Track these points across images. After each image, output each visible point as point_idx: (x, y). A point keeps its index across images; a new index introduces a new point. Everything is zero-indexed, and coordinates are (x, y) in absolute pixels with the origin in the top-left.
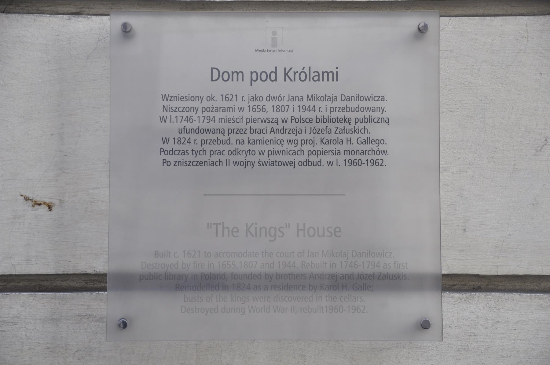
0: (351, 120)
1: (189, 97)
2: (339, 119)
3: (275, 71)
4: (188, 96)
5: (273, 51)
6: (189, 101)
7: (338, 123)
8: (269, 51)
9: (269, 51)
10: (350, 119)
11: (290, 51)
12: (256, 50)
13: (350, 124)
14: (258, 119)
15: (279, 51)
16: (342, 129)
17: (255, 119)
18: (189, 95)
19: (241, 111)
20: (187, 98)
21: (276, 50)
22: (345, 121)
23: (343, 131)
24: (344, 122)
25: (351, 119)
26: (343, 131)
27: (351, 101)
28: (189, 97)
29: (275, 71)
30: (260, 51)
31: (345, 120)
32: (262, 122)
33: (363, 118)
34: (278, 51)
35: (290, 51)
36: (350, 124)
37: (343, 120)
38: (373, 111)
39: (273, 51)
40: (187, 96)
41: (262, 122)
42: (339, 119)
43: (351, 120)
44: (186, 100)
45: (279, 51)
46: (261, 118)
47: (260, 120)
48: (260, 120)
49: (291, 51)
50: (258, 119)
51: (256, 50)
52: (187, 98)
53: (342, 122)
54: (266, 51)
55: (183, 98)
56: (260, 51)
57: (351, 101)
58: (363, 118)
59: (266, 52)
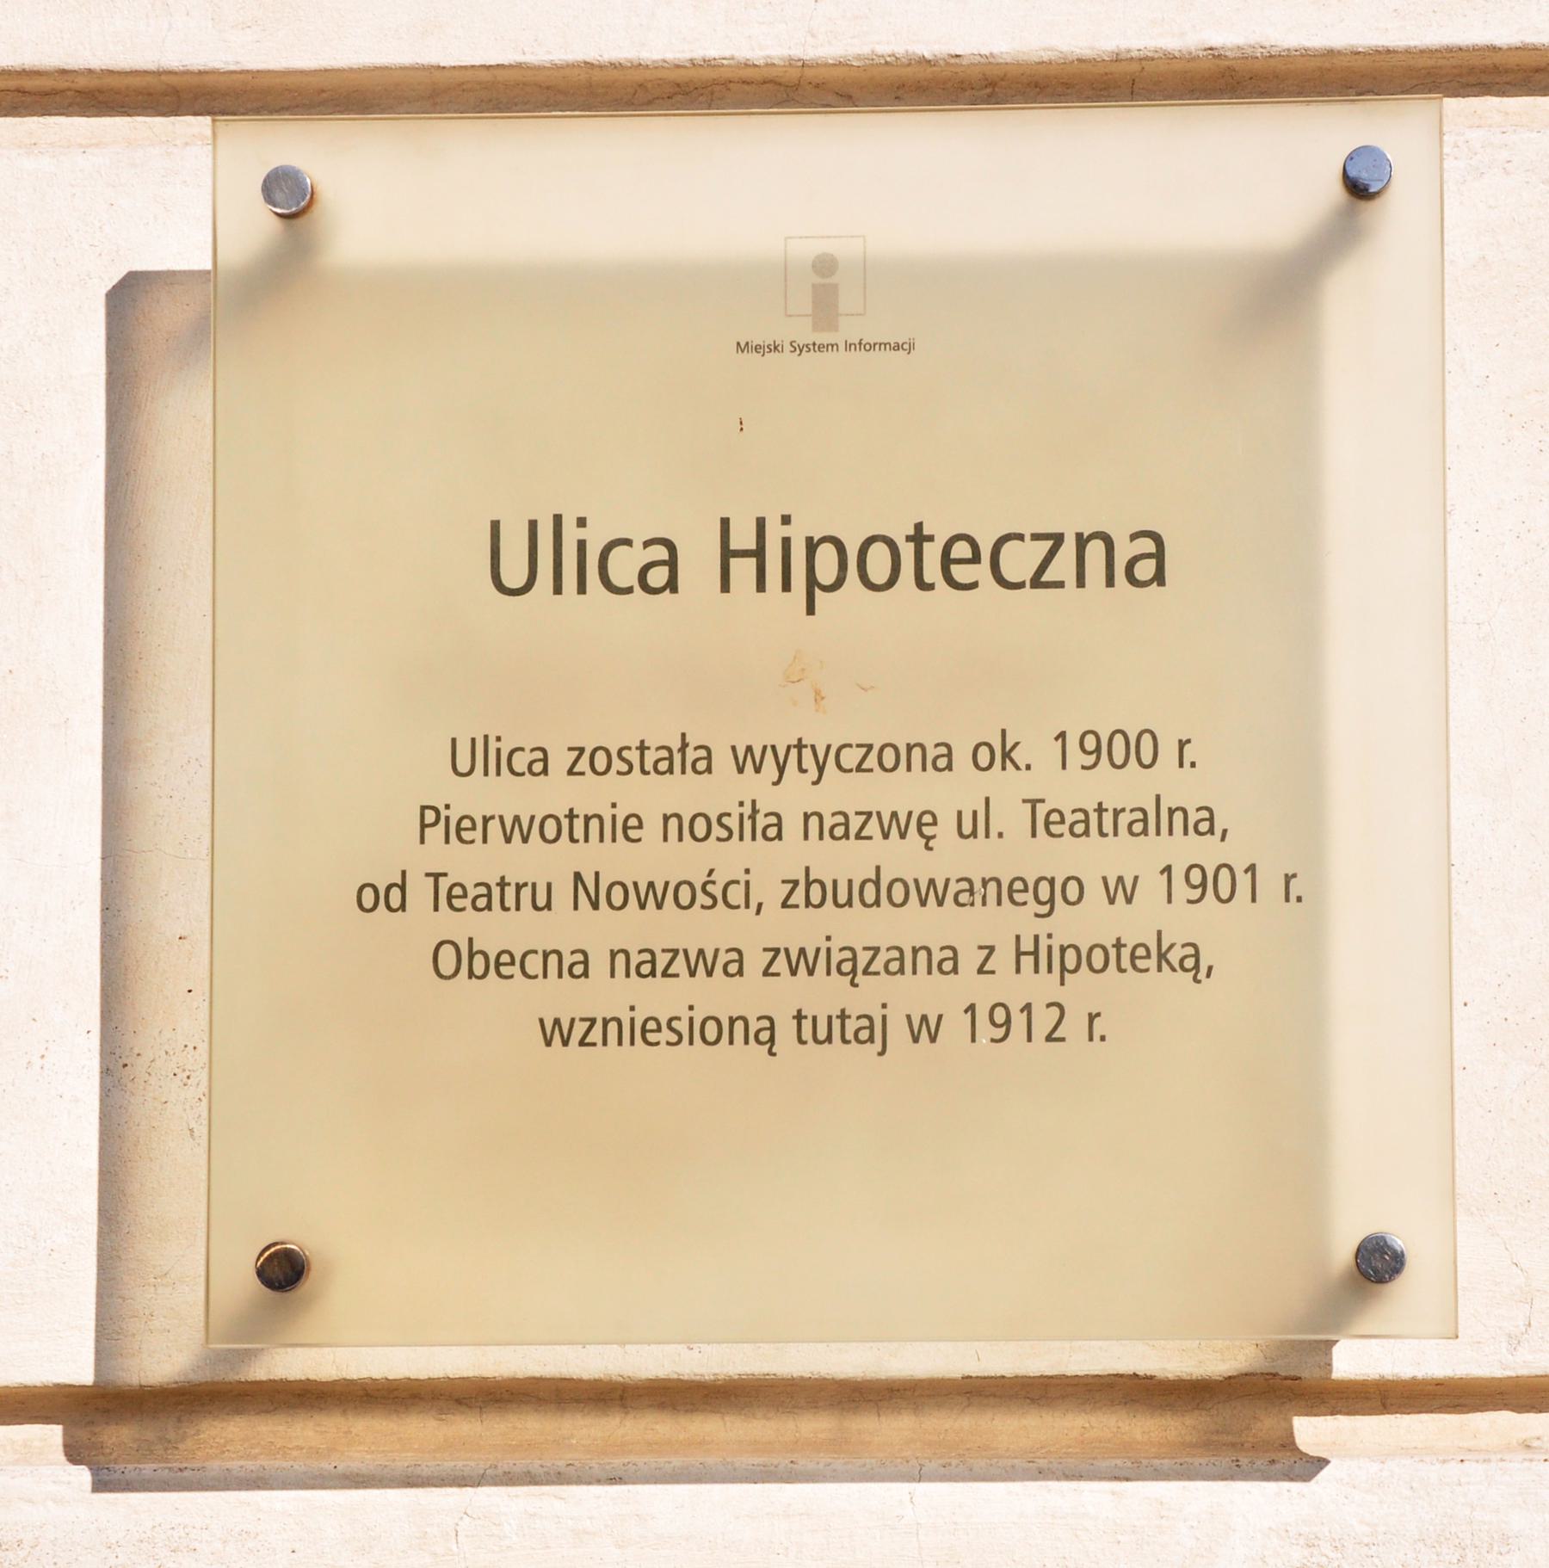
0: (935, 823)
1: (691, 1019)
2: (1126, 953)
3: (817, 590)
4: (686, 1014)
5: (821, 348)
6: (691, 1042)
7: (1124, 971)
8: (798, 349)
9: (798, 349)
10: (927, 819)
11: (897, 347)
12: (738, 344)
13: (931, 844)
14: (486, 820)
15: (849, 346)
16: (669, 750)
17: (466, 823)
18: (691, 1008)
19: (517, 836)
20: (683, 1026)
21: (833, 346)
22: (1164, 964)
23: (677, 758)
24: (1160, 969)
25: (934, 816)
26: (677, 758)
27: (1171, 832)
28: (691, 1019)
29: (817, 590)
30: (757, 348)
31: (1162, 956)
32: (508, 840)
33: (975, 813)
34: (842, 347)
35: (897, 347)
36: (931, 844)
37: (1148, 956)
38: (1132, 833)
39: (821, 348)
40: (678, 1019)
41: (508, 840)
42: (1126, 953)
43: (935, 823)
44: (674, 1038)
45: (849, 346)
46: (501, 818)
47: (494, 826)
48: (494, 826)
49: (906, 346)
50: (486, 820)
51: (738, 344)
52: (683, 1026)
53: (1147, 970)
54: (788, 348)
55: (659, 1030)
56: (757, 348)
57: (1171, 832)
58: (975, 813)
59: (787, 356)
